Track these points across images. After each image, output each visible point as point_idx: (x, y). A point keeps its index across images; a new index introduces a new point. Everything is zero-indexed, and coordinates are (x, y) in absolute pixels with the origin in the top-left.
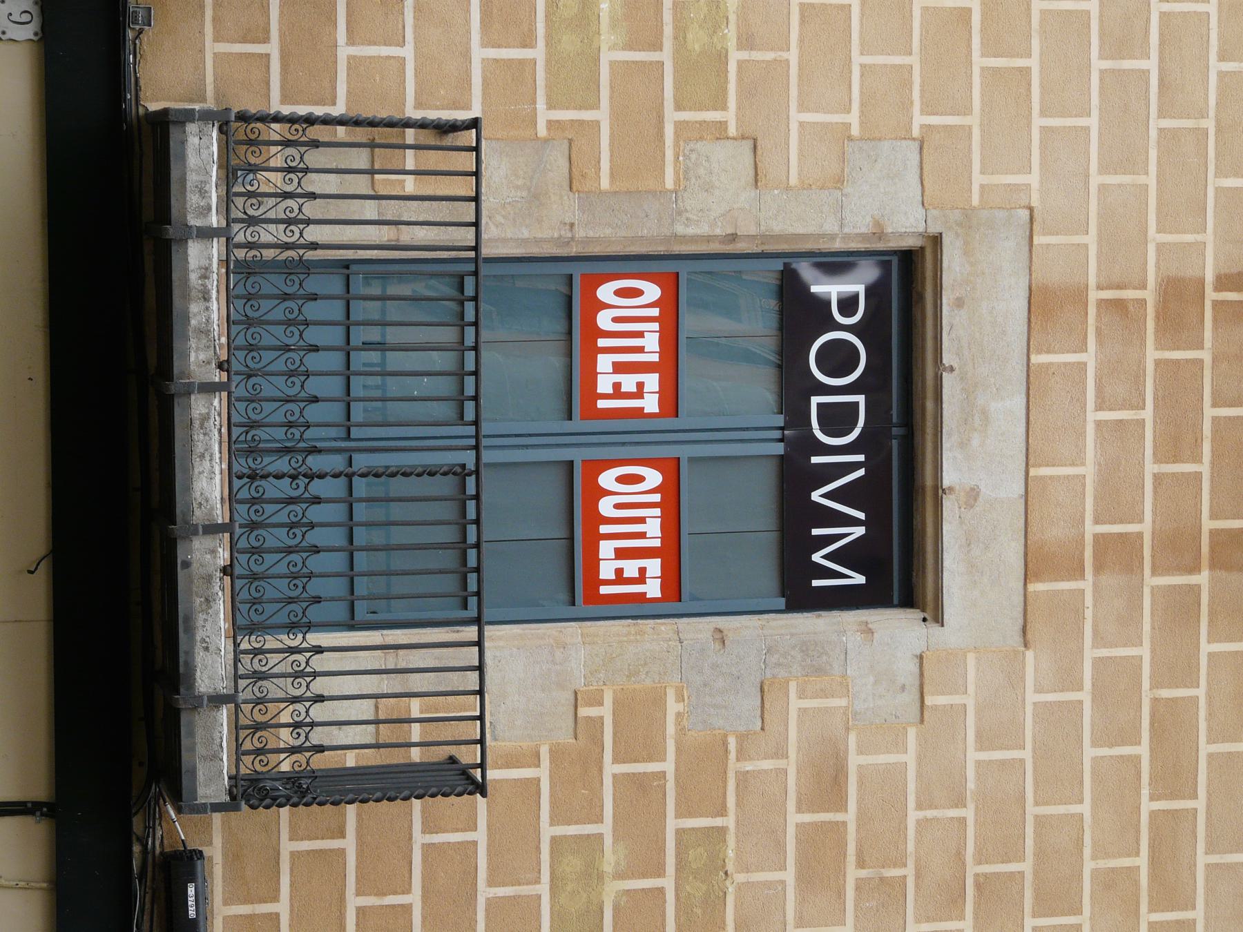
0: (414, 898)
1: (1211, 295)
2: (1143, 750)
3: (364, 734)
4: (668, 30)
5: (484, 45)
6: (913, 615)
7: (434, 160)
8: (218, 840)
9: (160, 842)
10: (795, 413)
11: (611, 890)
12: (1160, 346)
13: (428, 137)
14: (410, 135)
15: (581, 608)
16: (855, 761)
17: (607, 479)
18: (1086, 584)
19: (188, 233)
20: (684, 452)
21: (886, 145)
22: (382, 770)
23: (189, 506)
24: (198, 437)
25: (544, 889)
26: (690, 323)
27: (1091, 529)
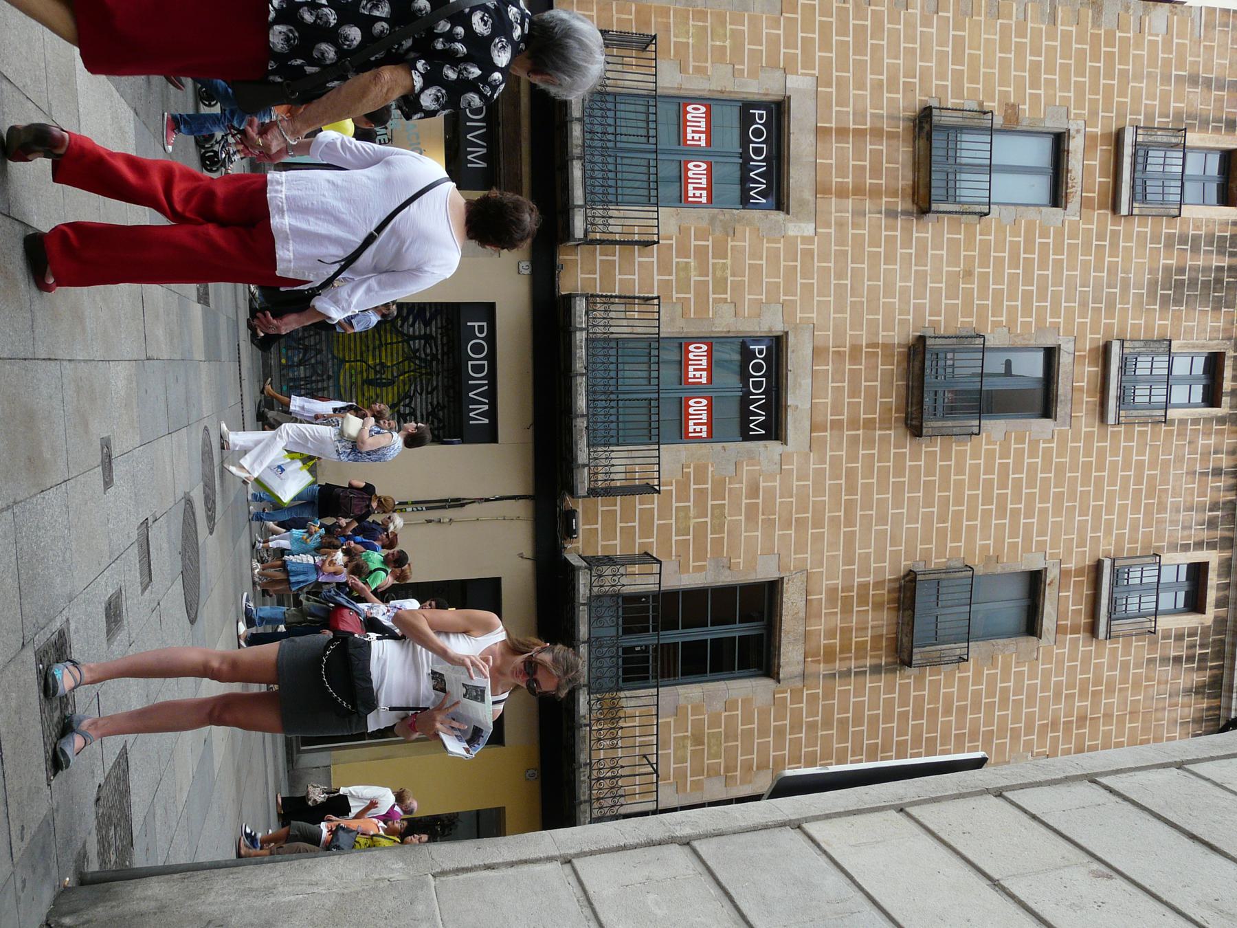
1: (864, 350)
3: (622, 476)
5: (658, 275)
6: (779, 442)
7: (644, 308)
8: (581, 507)
10: (746, 385)
11: (693, 521)
12: (850, 364)
13: (641, 301)
14: (637, 301)
16: (762, 485)
17: (691, 402)
18: (828, 434)
19: (577, 329)
20: (714, 395)
23: (576, 409)
25: (673, 521)
27: (829, 417)
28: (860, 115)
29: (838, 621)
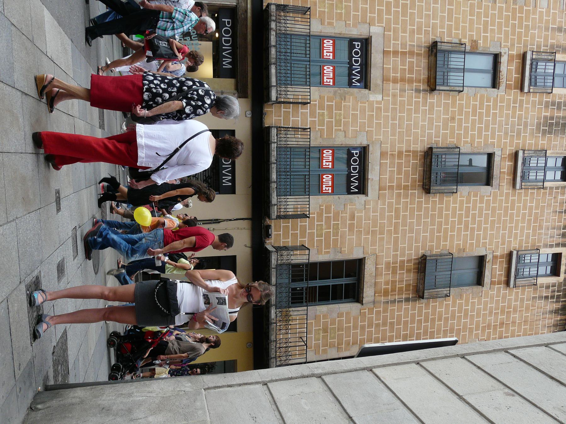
0: (298, 232)
2: (393, 214)
3: (292, 210)
4: (334, 116)
5: (310, 118)
6: (364, 195)
7: (303, 133)
8: (273, 224)
9: (265, 224)
11: (324, 231)
13: (302, 130)
14: (300, 130)
15: (321, 194)
16: (356, 215)
17: (324, 177)
19: (272, 142)
20: (334, 173)
21: (362, 132)
22: (461, 53)
24: (273, 170)
25: (315, 231)
26: (335, 155)
27: (388, 184)
28: (404, 45)
29: (390, 277)
